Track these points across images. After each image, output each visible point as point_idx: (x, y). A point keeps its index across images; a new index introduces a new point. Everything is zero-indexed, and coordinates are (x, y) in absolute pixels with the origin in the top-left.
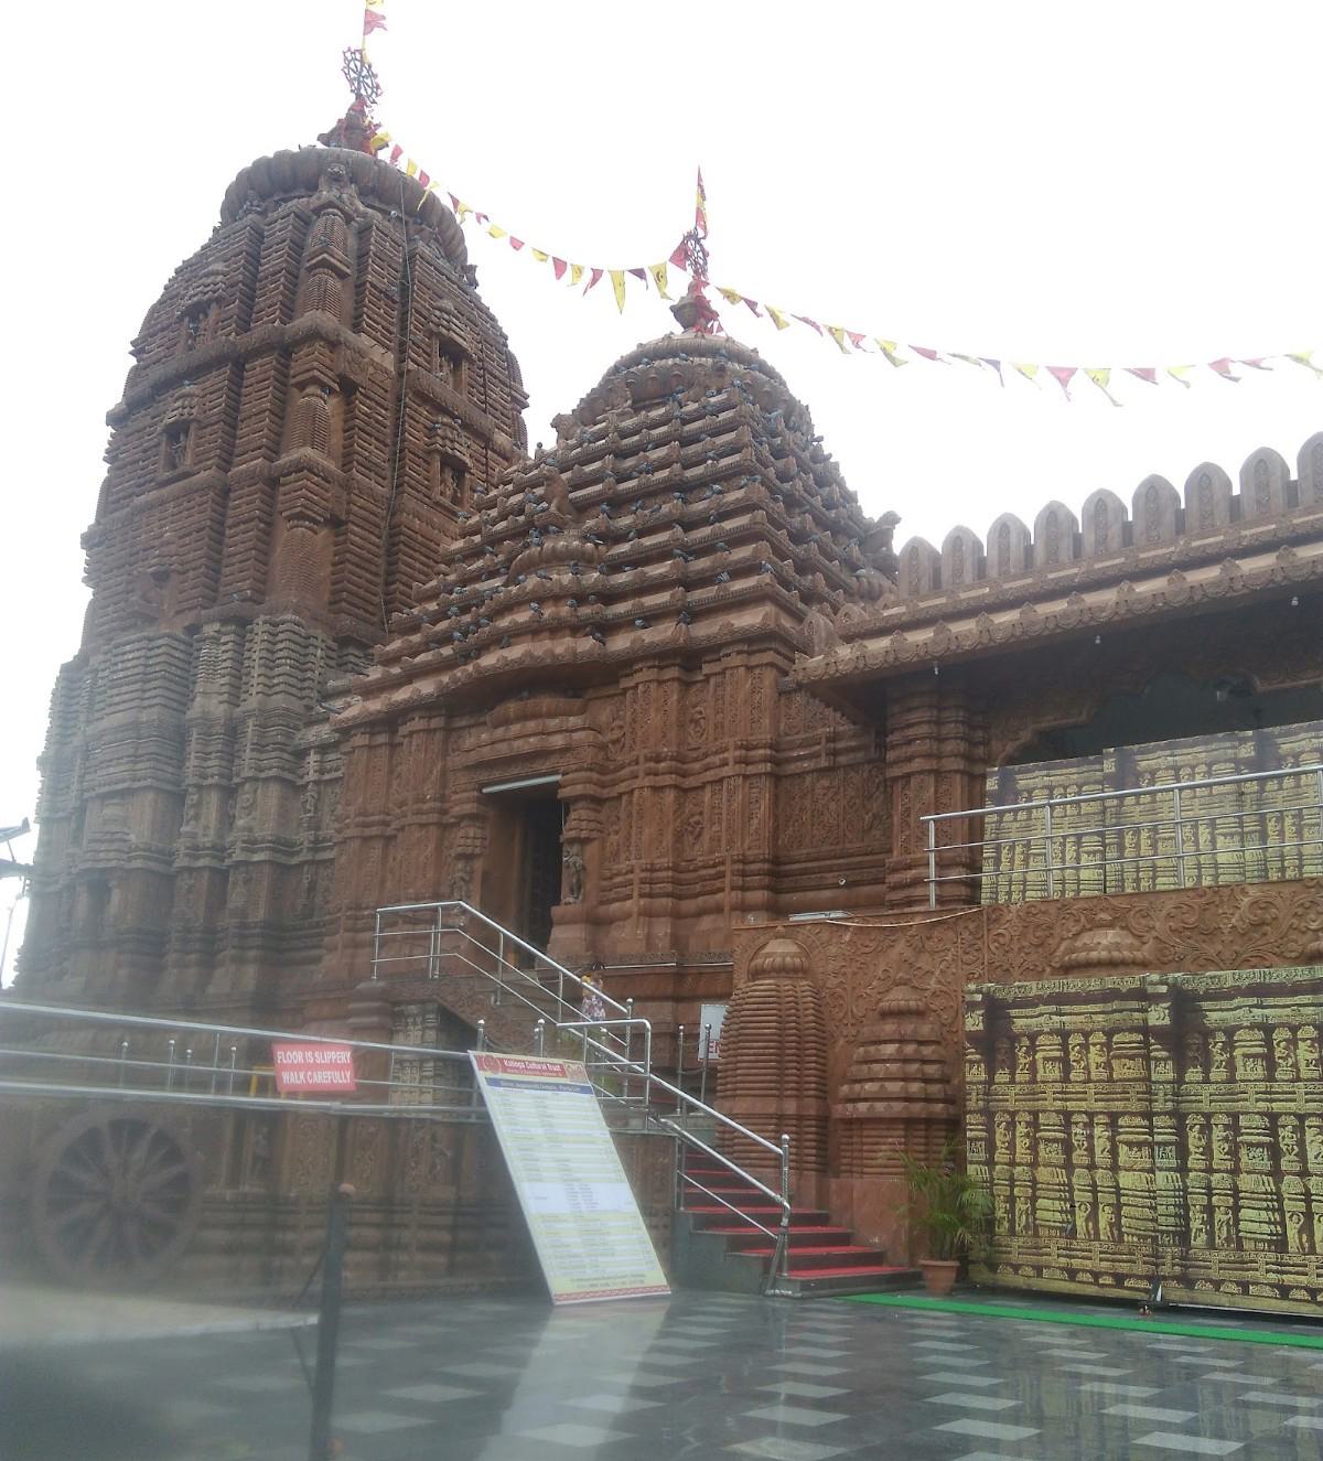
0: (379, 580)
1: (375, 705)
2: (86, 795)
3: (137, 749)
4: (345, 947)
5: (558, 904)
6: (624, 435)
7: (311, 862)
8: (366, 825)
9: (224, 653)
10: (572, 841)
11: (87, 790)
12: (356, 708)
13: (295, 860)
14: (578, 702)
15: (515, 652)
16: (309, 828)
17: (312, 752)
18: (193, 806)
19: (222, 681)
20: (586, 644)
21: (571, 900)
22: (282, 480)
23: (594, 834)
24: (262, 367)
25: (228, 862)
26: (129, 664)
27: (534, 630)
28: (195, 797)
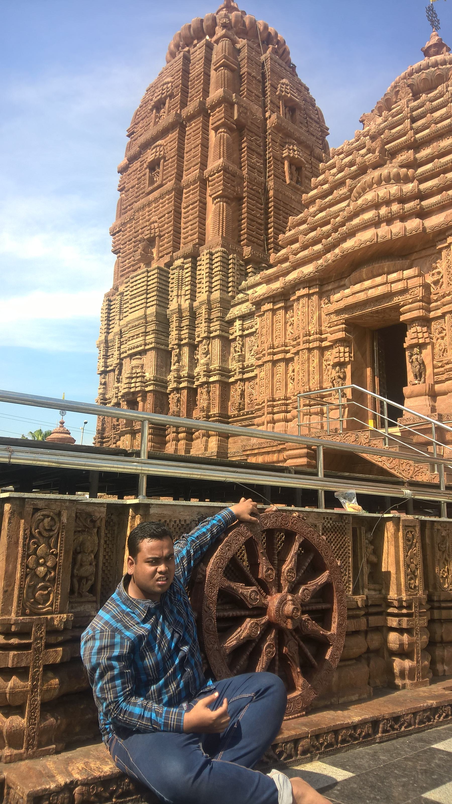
0: (262, 227)
1: (277, 285)
2: (122, 356)
3: (146, 328)
4: (268, 423)
5: (406, 385)
6: (413, 110)
7: (242, 380)
8: (274, 354)
9: (187, 273)
10: (412, 347)
11: (123, 353)
12: (262, 290)
13: (232, 380)
14: (408, 262)
15: (366, 236)
16: (239, 361)
17: (237, 320)
18: (176, 355)
19: (187, 288)
20: (413, 224)
21: (416, 382)
22: (210, 178)
23: (428, 340)
24: (193, 128)
25: (197, 383)
26: (139, 286)
27: (376, 223)
28: (178, 350)
